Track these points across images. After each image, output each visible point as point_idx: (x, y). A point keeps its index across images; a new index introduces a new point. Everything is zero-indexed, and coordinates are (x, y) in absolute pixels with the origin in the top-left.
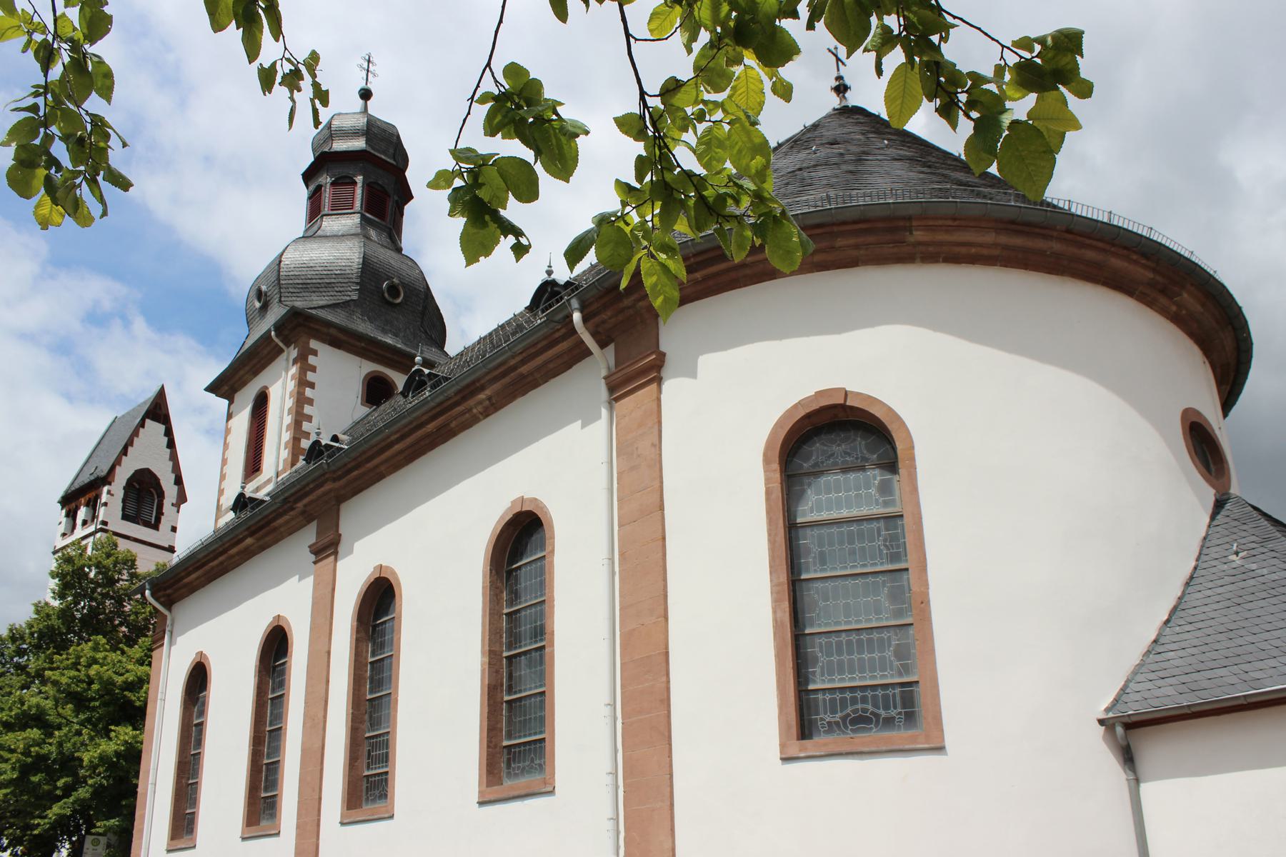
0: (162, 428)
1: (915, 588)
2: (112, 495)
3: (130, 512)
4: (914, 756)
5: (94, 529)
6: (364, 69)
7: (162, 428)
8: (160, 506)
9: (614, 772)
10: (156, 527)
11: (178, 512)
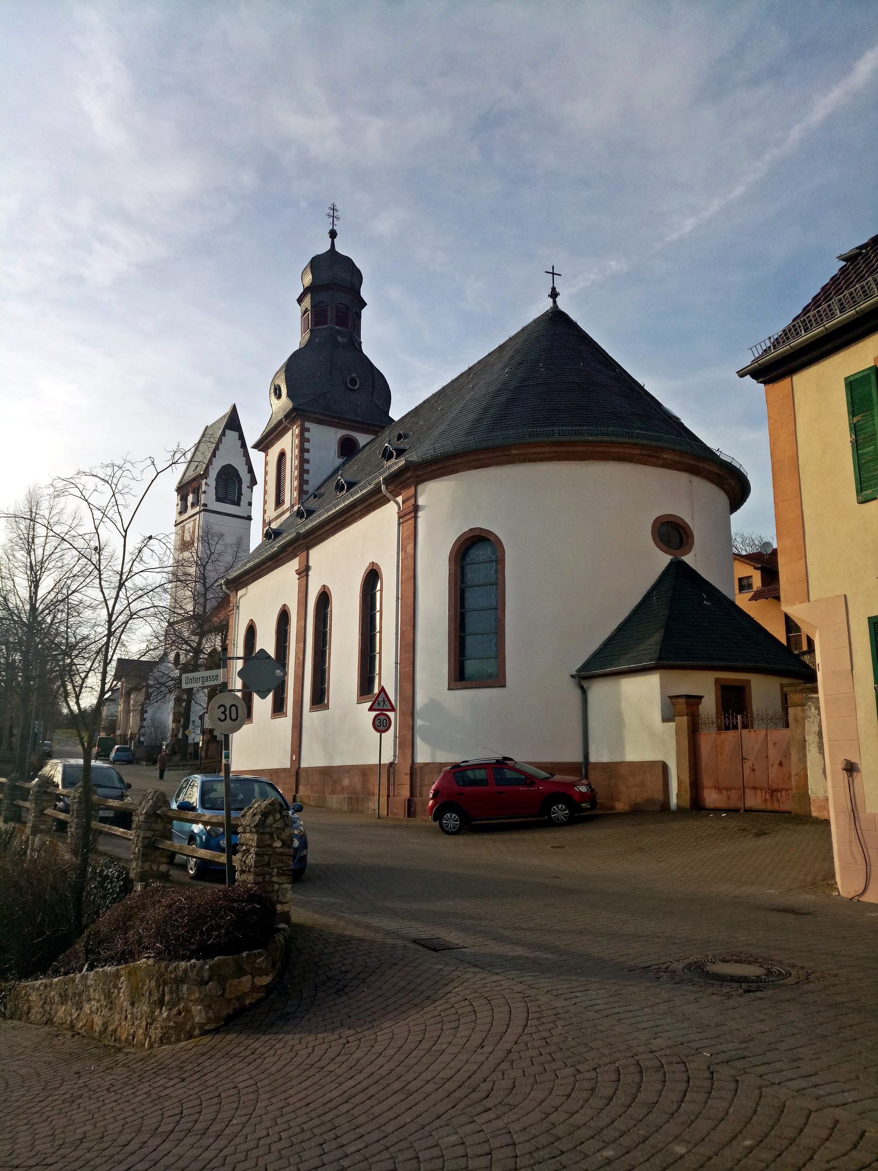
0: (236, 434)
3: (220, 495)
4: (653, 674)
6: (331, 216)
7: (236, 434)
8: (240, 489)
10: (238, 503)
11: (252, 491)
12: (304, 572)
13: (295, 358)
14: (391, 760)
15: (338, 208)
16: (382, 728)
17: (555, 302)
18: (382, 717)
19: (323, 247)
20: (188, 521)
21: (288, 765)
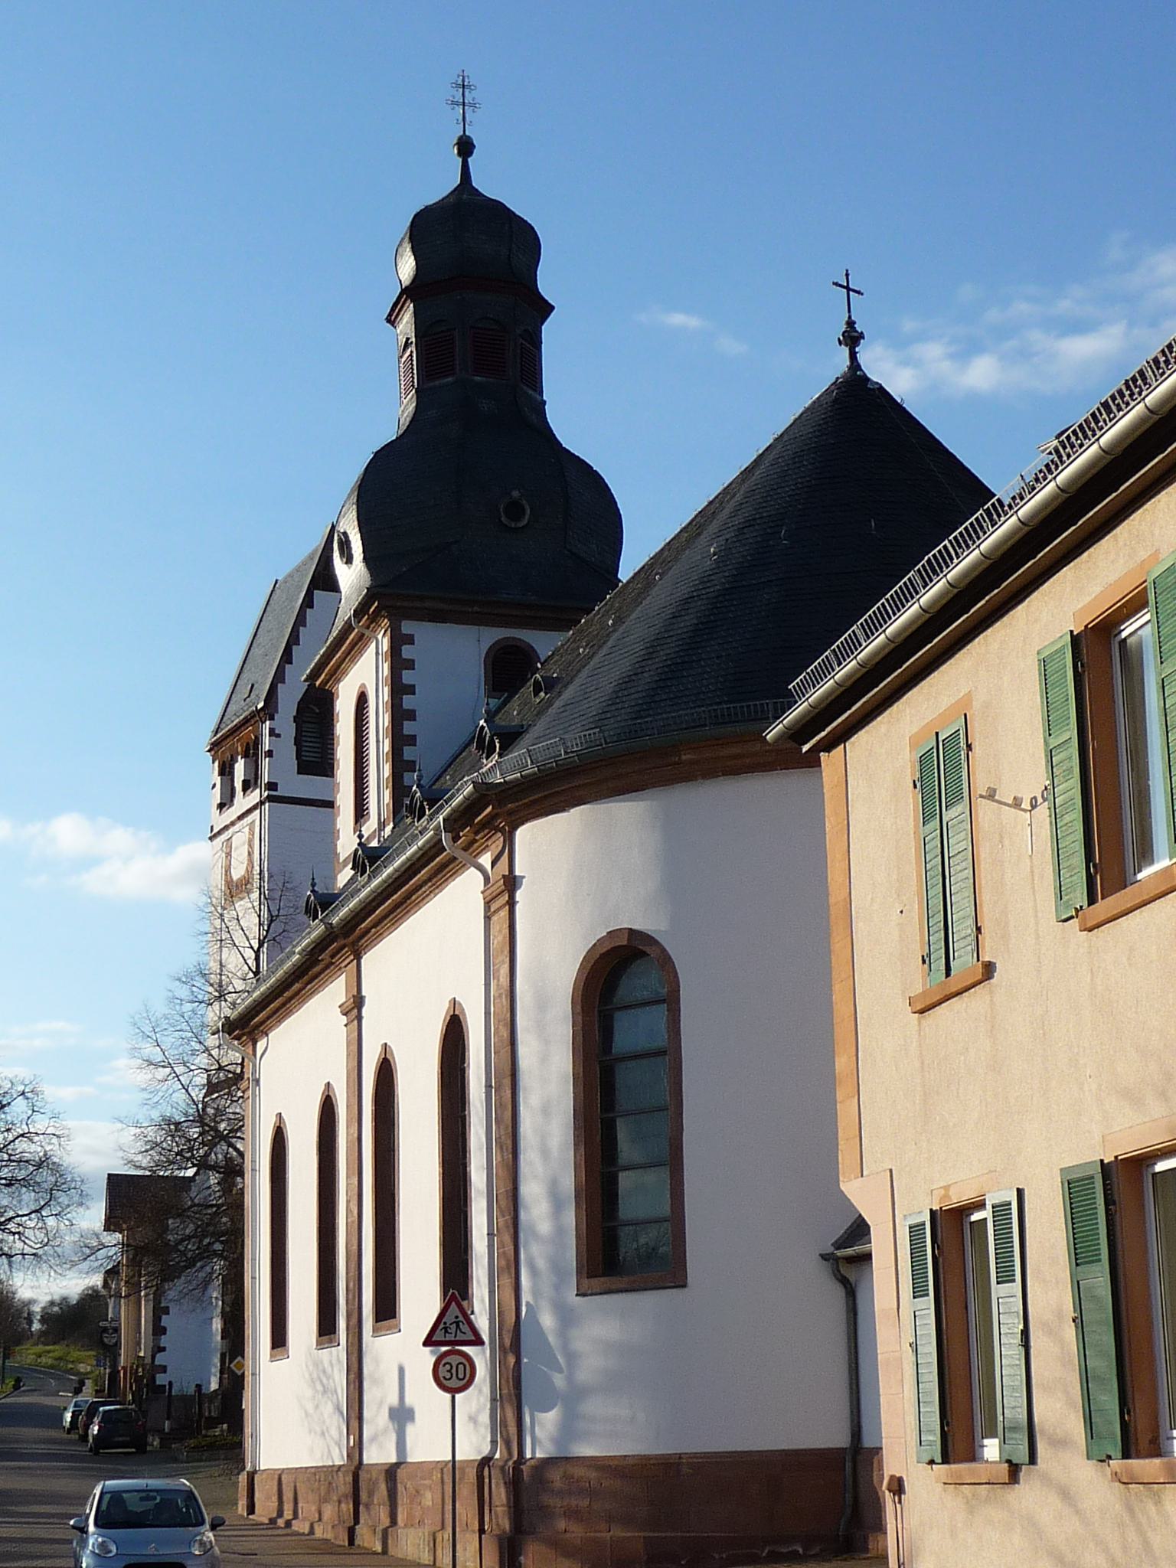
1: (616, 1463)
2: (278, 736)
5: (258, 800)
9: (149, 1488)
12: (355, 1007)
13: (383, 462)
14: (486, 1450)
15: (471, 80)
16: (454, 1383)
17: (853, 356)
18: (454, 1360)
19: (440, 184)
20: (236, 828)
21: (339, 1461)
